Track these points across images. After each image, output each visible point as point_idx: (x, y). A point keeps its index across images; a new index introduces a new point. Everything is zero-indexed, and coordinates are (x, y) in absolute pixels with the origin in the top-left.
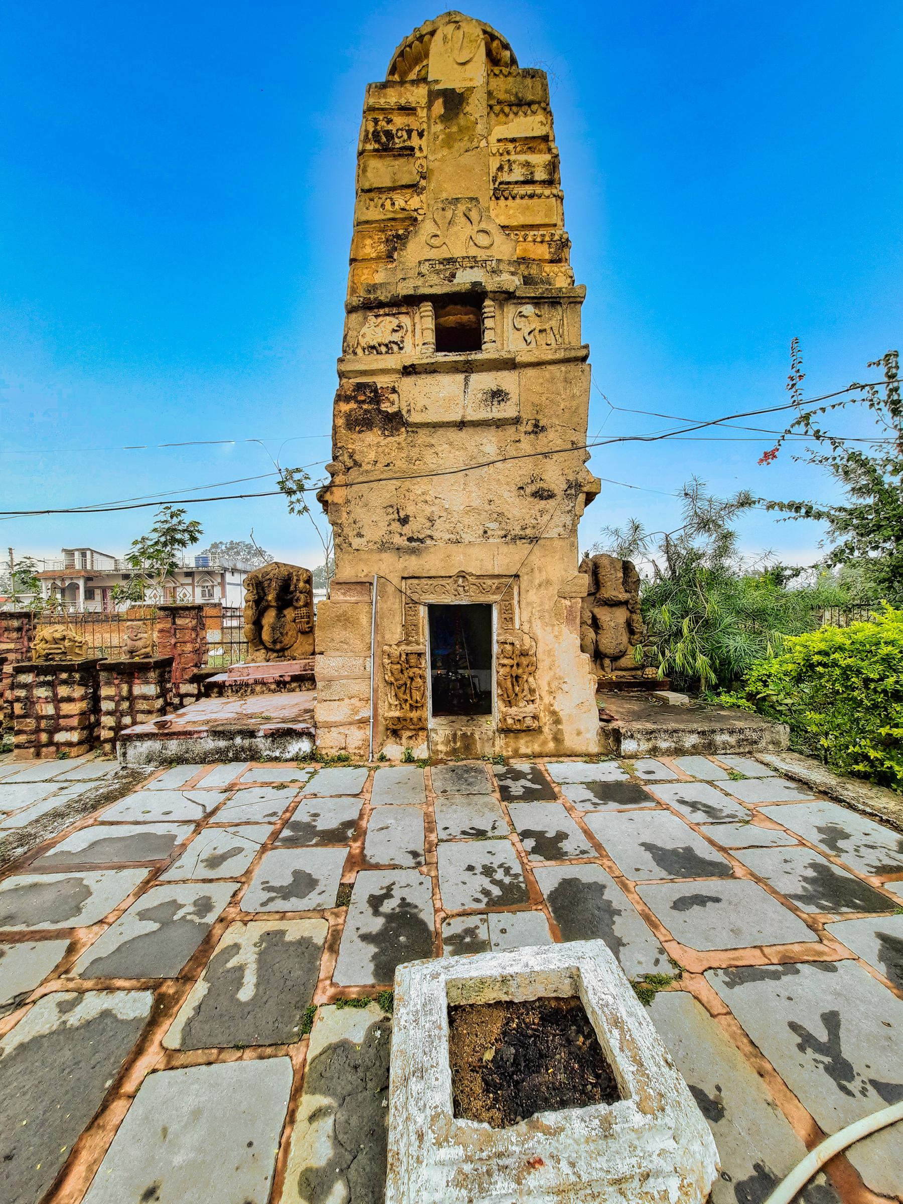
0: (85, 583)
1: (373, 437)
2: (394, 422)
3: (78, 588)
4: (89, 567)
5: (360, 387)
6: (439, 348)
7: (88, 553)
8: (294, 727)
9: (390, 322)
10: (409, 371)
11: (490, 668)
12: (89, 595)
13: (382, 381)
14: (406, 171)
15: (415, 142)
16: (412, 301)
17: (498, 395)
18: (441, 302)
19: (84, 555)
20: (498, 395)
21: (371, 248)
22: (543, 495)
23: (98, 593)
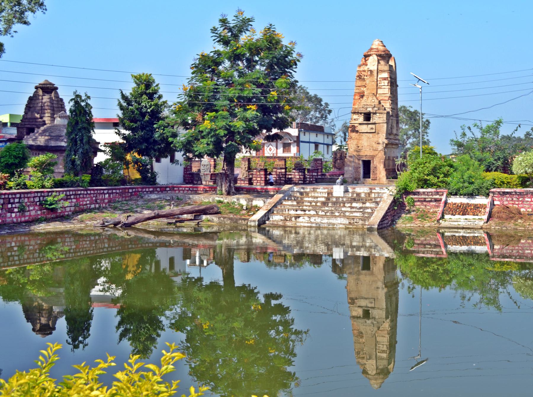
1: (354, 134)
2: (357, 132)
5: (353, 126)
8: (464, 200)
9: (357, 116)
10: (360, 124)
11: (370, 174)
13: (356, 125)
14: (364, 83)
15: (365, 77)
16: (361, 113)
17: (372, 129)
20: (372, 129)
22: (378, 144)
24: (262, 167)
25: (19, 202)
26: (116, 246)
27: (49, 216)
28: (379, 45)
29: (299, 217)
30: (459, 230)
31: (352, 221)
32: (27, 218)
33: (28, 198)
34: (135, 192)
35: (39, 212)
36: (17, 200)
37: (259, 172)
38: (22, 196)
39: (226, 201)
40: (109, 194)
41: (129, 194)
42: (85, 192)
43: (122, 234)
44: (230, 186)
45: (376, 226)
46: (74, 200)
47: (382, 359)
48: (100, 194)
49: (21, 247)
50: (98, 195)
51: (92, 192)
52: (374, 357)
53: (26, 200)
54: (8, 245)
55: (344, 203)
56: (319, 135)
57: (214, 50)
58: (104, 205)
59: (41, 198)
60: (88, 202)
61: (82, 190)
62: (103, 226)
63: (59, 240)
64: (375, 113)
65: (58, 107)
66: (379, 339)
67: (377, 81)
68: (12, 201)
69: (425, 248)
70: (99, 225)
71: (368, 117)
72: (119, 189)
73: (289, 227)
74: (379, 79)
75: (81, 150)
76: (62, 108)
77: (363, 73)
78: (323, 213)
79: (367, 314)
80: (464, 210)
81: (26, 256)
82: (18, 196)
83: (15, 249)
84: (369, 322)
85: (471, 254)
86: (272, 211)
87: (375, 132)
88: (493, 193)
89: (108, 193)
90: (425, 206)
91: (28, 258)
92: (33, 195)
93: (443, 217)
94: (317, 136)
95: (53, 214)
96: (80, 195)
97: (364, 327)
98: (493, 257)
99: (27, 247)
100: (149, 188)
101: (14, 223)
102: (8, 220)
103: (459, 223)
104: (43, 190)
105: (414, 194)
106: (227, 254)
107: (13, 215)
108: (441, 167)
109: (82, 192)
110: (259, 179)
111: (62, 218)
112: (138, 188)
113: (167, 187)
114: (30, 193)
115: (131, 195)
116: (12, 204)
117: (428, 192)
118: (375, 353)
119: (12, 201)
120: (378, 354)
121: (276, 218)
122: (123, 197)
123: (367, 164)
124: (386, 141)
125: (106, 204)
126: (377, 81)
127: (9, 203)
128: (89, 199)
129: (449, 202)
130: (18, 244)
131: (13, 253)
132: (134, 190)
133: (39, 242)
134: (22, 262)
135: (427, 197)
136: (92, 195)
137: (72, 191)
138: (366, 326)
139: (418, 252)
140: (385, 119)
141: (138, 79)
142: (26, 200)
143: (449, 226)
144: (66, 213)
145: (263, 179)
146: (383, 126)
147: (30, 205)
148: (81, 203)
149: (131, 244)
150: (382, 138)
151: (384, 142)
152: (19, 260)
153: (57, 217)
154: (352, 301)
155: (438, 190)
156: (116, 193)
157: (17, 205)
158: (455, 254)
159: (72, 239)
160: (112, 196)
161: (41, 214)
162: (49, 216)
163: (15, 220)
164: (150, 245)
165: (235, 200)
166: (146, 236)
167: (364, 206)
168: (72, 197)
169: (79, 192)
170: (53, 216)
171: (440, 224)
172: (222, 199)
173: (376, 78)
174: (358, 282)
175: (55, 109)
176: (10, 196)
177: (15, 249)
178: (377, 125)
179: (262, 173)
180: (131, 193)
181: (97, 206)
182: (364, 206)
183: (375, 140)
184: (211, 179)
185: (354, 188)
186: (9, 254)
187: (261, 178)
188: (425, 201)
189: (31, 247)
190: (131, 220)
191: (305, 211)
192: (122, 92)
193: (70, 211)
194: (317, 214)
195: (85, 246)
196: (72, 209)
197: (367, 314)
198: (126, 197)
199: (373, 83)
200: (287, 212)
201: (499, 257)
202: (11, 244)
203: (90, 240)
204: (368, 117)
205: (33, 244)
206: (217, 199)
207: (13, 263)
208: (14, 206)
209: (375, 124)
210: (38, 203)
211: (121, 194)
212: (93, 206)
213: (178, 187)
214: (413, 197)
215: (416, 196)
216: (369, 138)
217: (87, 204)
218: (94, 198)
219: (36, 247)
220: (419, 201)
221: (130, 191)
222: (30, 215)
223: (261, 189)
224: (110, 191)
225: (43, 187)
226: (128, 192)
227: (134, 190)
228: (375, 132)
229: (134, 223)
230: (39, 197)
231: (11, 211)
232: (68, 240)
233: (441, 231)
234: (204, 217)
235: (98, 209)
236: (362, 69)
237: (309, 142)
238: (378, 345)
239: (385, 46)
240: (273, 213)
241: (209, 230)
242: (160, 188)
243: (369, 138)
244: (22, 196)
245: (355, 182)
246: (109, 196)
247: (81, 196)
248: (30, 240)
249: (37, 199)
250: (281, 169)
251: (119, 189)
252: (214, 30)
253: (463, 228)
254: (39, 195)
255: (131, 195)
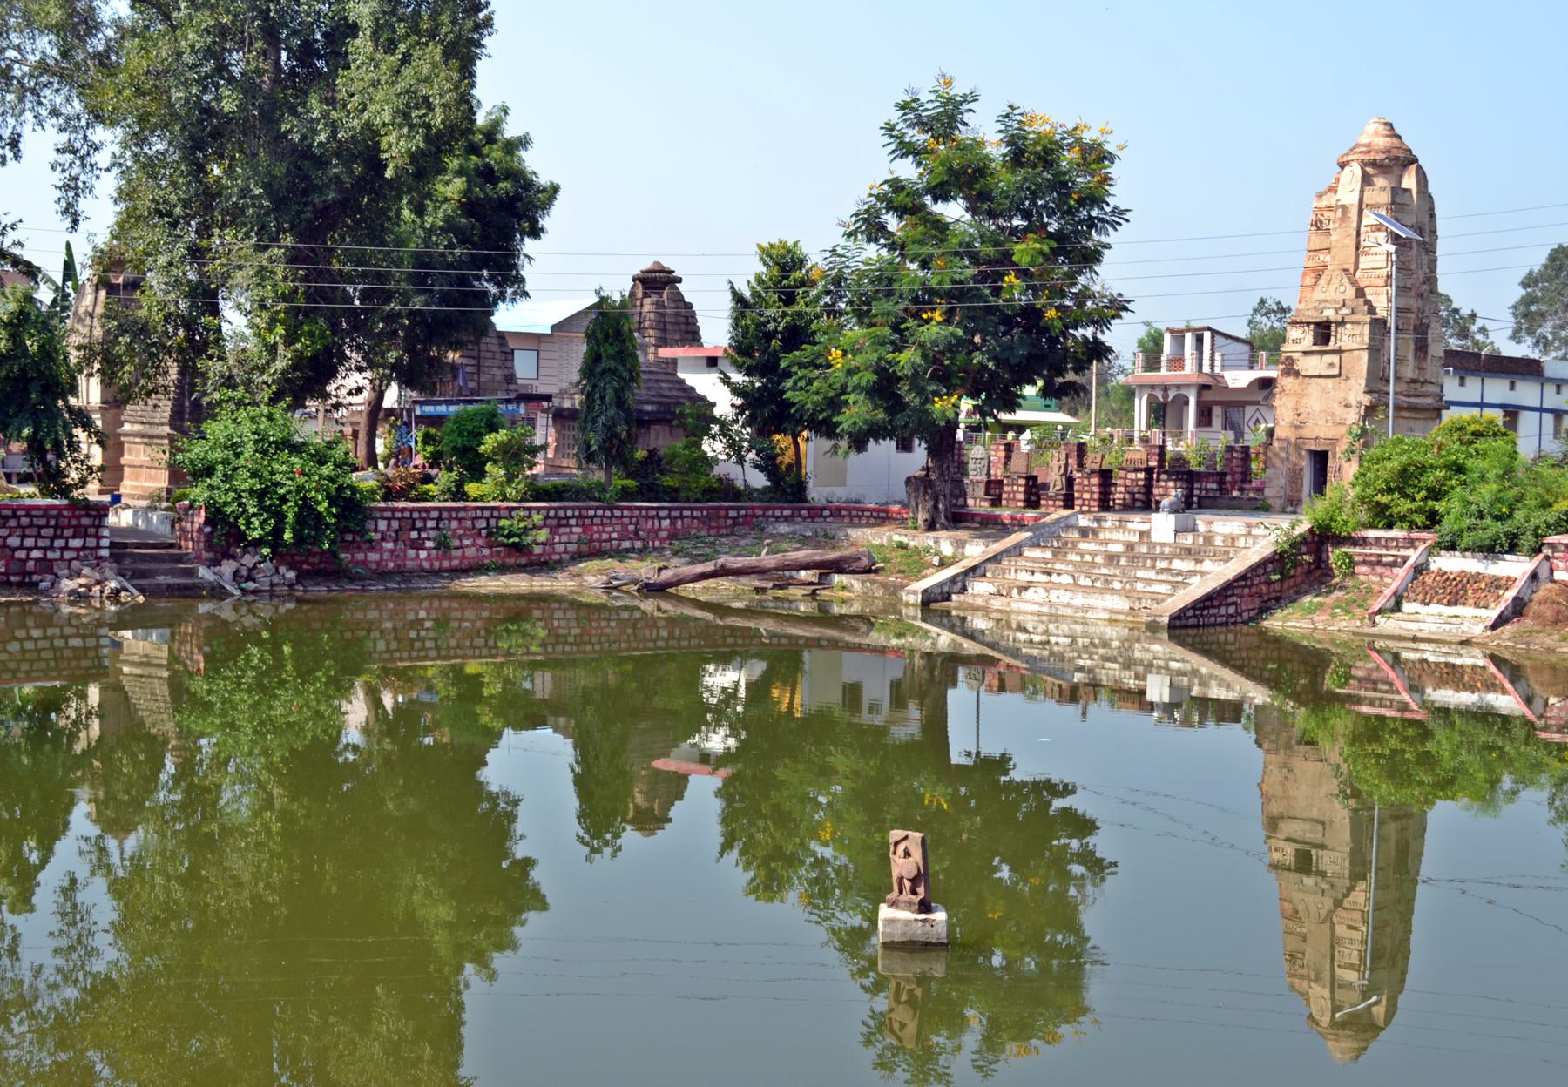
0: (1199, 395)
1: (1290, 379)
2: (1297, 374)
3: (1187, 403)
4: (1206, 369)
6: (1315, 344)
7: (1207, 336)
9: (1300, 331)
10: (1306, 353)
12: (1204, 418)
13: (1295, 356)
16: (1308, 324)
17: (1332, 365)
18: (1317, 324)
19: (1199, 340)
21: (1309, 281)
22: (1347, 406)
23: (1217, 412)
24: (1097, 467)
25: (437, 528)
26: (691, 637)
27: (512, 561)
28: (1376, 134)
29: (1026, 589)
30: (1422, 646)
31: (1137, 606)
32: (455, 563)
33: (460, 520)
34: (746, 516)
35: (486, 552)
36: (431, 524)
37: (1088, 478)
38: (445, 515)
39: (912, 543)
40: (673, 520)
41: (730, 522)
42: (608, 513)
43: (648, 605)
44: (935, 507)
45: (1166, 620)
46: (578, 530)
47: (1349, 986)
48: (647, 517)
49: (442, 623)
50: (642, 522)
51: (626, 513)
52: (1327, 976)
53: (454, 524)
54: (411, 616)
55: (1154, 560)
56: (1520, 385)
57: (889, 177)
58: (657, 543)
59: (492, 522)
60: (614, 535)
61: (597, 508)
62: (609, 588)
63: (537, 613)
64: (1342, 323)
65: (677, 324)
66: (1341, 930)
67: (1358, 234)
68: (419, 524)
69: (1375, 690)
70: (599, 584)
71: (1323, 332)
72: (701, 509)
73: (997, 611)
74: (1363, 229)
75: (602, 419)
76: (688, 324)
77: (1326, 214)
78: (1088, 582)
79: (1304, 863)
80: (1456, 591)
81: (453, 643)
82: (435, 514)
83: (428, 624)
84: (1309, 881)
85: (1484, 716)
86: (979, 572)
87: (1339, 375)
88: (1552, 546)
89: (669, 516)
90: (1381, 576)
91: (458, 647)
92: (471, 514)
93: (1397, 608)
94: (1558, 392)
95: (518, 556)
96: (592, 518)
97: (1301, 895)
98: (1546, 729)
99: (456, 624)
100: (782, 509)
101: (423, 570)
102: (410, 564)
103: (1422, 626)
104: (461, 504)
105: (1355, 542)
106: (926, 674)
107: (423, 554)
108: (1422, 469)
109: (600, 512)
110: (1086, 496)
111: (543, 566)
112: (753, 508)
113: (824, 508)
114: (465, 509)
115: (735, 524)
116: (420, 530)
117: (1387, 540)
118: (1328, 967)
119: (419, 524)
120: (1338, 971)
121: (980, 588)
122: (710, 527)
123: (1320, 459)
124: (1366, 400)
125: (662, 541)
126: (1358, 234)
127: (414, 528)
128: (618, 528)
129: (1433, 567)
130: (433, 616)
131: (423, 633)
132: (743, 512)
133: (485, 614)
134: (443, 653)
135: (1384, 552)
136: (626, 521)
137: (573, 508)
138: (1308, 895)
139: (1359, 700)
140: (1366, 339)
141: (767, 253)
142: (454, 524)
143: (1397, 632)
144: (556, 557)
145: (1096, 496)
146: (1359, 358)
147: (465, 535)
148: (596, 536)
149: (731, 636)
150: (1356, 392)
151: (1360, 403)
152: (437, 648)
153: (531, 564)
154: (1272, 823)
155: (1414, 535)
156: (693, 518)
157: (433, 534)
158: (1444, 712)
159: (571, 614)
160: (679, 523)
161: (492, 555)
162: (512, 561)
163: (426, 565)
164: (783, 641)
165: (931, 543)
166: (699, 614)
167: (1198, 567)
168: (572, 522)
169: (591, 513)
170: (523, 560)
171: (1374, 624)
172: (905, 540)
173: (1354, 225)
174: (1290, 776)
175: (669, 327)
176: (416, 515)
177: (428, 624)
178: (1344, 356)
179: (1095, 480)
180: (734, 518)
181: (638, 544)
182: (1198, 567)
183: (1341, 395)
184: (987, 493)
185: (1211, 523)
186: (413, 634)
187: (1092, 493)
188: (1379, 563)
189: (466, 624)
190: (666, 575)
191: (1050, 574)
192: (732, 287)
193: (566, 552)
194: (1076, 584)
195: (608, 631)
196: (572, 548)
197: (1304, 863)
198: (718, 528)
199: (1347, 241)
200: (1013, 576)
201: (1558, 732)
202: (417, 613)
203: (619, 620)
204: (1323, 332)
205: (470, 618)
206: (896, 538)
207: (422, 653)
208: (424, 535)
209: (1339, 352)
210: (484, 533)
211: (705, 521)
212: (626, 544)
213: (850, 510)
214: (1351, 550)
215: (1357, 550)
216: (1324, 391)
217: (610, 540)
218: (631, 527)
219: (479, 624)
220: (1364, 563)
221: (732, 513)
222: (464, 557)
223: (1013, 518)
224: (675, 513)
225: (505, 499)
226: (727, 517)
227: (743, 512)
228: (1339, 375)
229: (671, 585)
230: (488, 519)
231: (418, 545)
232: (559, 614)
233: (1377, 645)
234: (837, 579)
235: (640, 551)
236: (1324, 203)
237: (1541, 410)
238: (1337, 948)
239: (1399, 137)
240: (984, 575)
241: (843, 611)
242: (809, 509)
243: (1324, 391)
244: (445, 515)
245: (1289, 509)
246: (673, 523)
247: (596, 521)
248: (463, 610)
249: (482, 524)
250: (1136, 470)
251: (701, 509)
252: (889, 128)
253: (1429, 641)
254: (487, 514)
255: (735, 524)
